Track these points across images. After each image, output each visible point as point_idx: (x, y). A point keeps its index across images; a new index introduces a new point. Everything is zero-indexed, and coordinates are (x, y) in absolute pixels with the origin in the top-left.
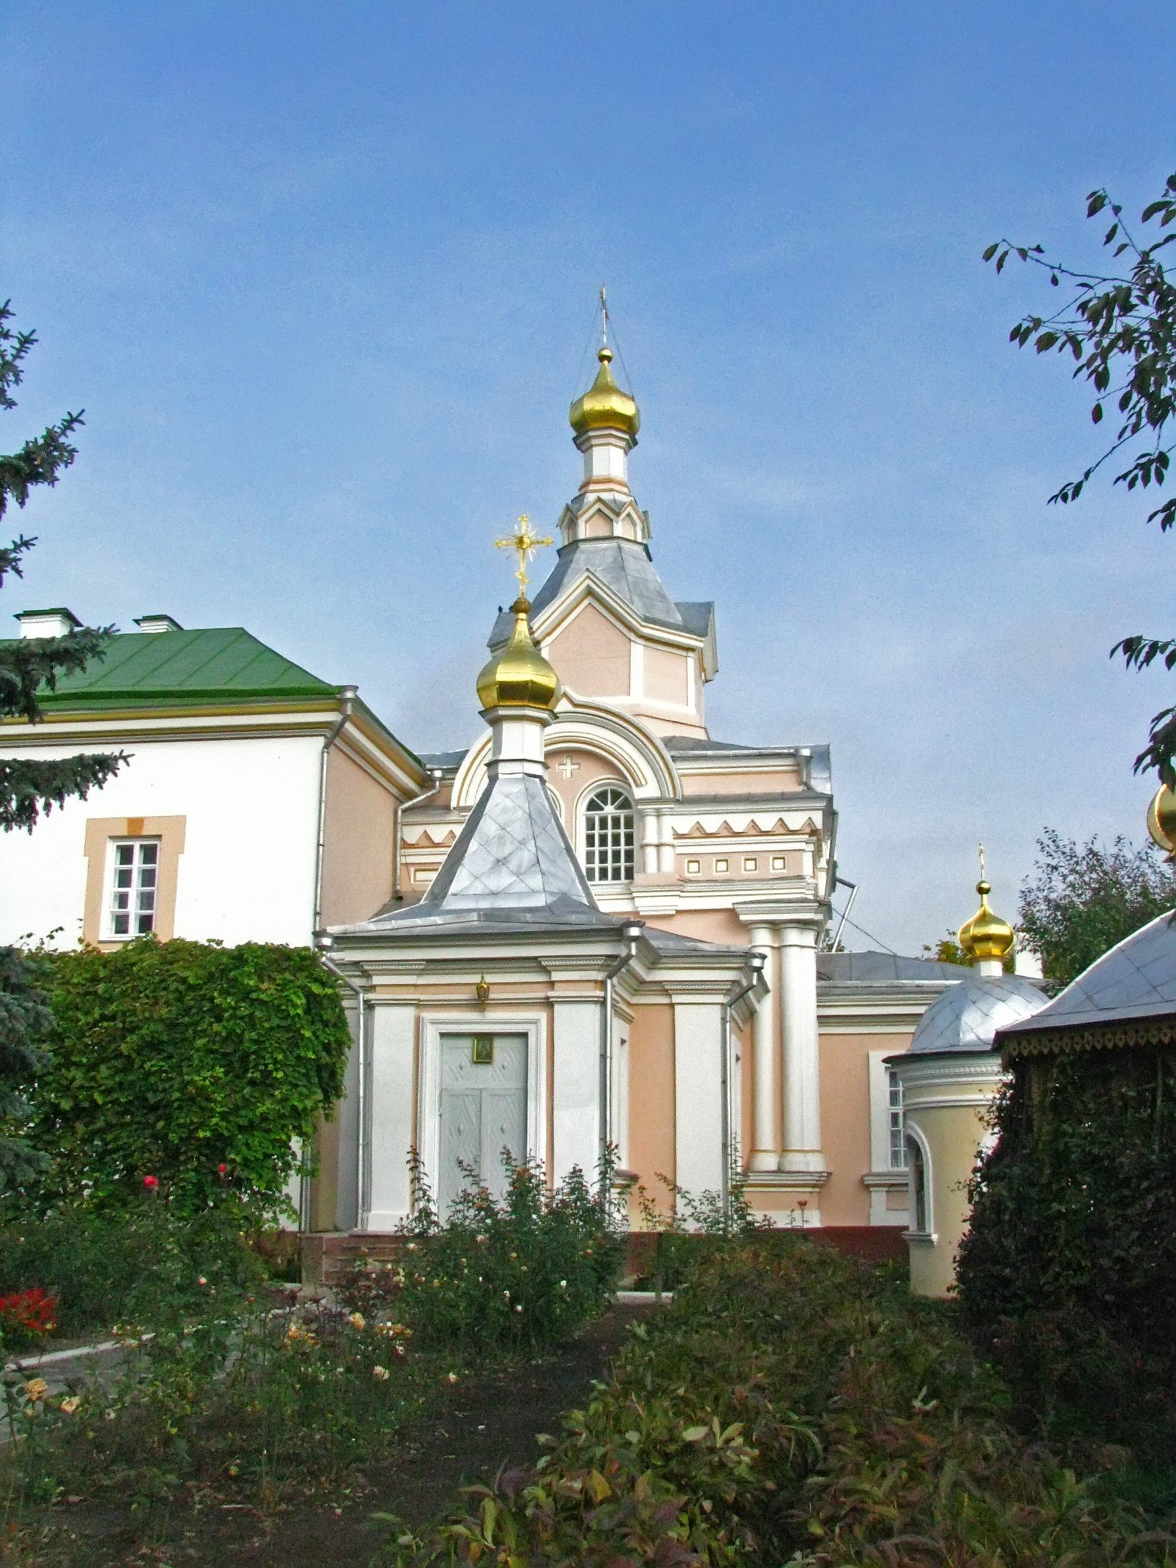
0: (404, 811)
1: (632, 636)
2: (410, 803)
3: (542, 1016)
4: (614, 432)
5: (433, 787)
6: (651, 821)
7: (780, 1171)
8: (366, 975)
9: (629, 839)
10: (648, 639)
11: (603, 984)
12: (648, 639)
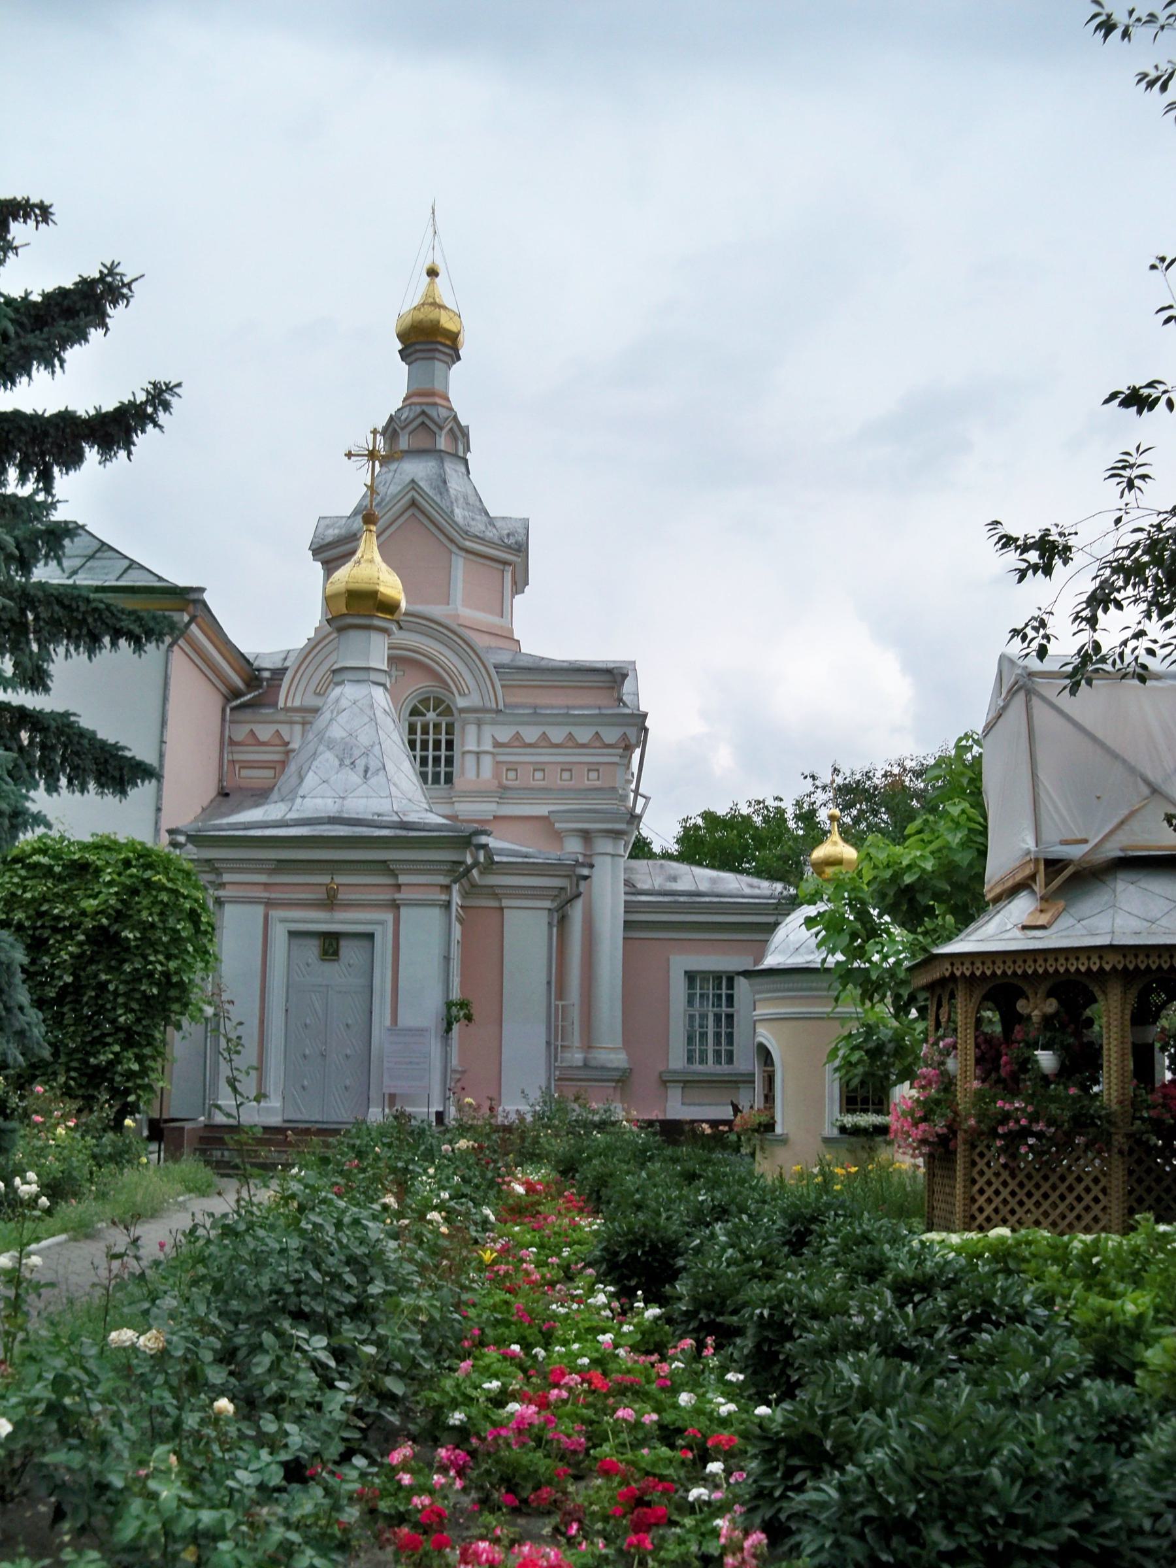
0: (232, 709)
1: (454, 549)
2: (238, 702)
3: (389, 917)
4: (418, 347)
5: (260, 686)
6: (472, 730)
7: (586, 1065)
8: (218, 872)
9: (450, 745)
10: (468, 551)
11: (447, 888)
12: (468, 551)
